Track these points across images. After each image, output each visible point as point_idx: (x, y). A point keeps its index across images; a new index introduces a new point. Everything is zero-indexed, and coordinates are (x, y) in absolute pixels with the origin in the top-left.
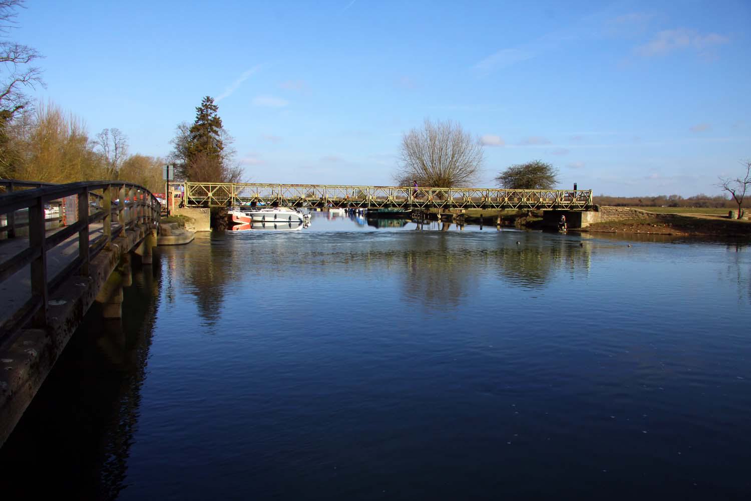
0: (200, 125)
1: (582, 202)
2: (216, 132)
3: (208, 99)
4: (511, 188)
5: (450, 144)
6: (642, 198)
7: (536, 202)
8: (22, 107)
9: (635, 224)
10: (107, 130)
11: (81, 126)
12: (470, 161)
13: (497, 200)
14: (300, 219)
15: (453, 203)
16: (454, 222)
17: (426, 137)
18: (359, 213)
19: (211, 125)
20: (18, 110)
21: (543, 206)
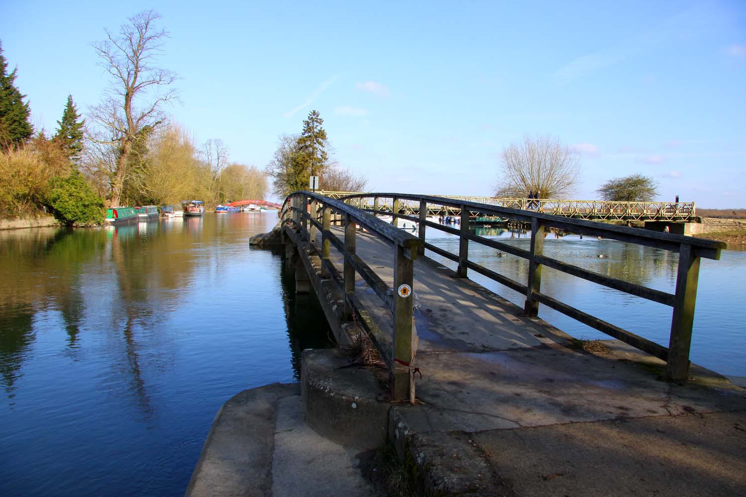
0: (306, 137)
1: (684, 214)
2: (320, 144)
3: (314, 113)
4: (611, 200)
5: (548, 157)
6: (736, 210)
7: (640, 214)
8: (160, 122)
9: (739, 235)
10: (211, 140)
11: (192, 138)
12: (567, 173)
13: (601, 211)
14: (413, 226)
15: (562, 213)
16: (551, 231)
17: (525, 149)
18: (455, 222)
19: (316, 137)
20: (157, 125)
21: (613, 217)
